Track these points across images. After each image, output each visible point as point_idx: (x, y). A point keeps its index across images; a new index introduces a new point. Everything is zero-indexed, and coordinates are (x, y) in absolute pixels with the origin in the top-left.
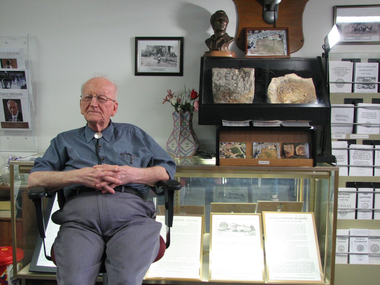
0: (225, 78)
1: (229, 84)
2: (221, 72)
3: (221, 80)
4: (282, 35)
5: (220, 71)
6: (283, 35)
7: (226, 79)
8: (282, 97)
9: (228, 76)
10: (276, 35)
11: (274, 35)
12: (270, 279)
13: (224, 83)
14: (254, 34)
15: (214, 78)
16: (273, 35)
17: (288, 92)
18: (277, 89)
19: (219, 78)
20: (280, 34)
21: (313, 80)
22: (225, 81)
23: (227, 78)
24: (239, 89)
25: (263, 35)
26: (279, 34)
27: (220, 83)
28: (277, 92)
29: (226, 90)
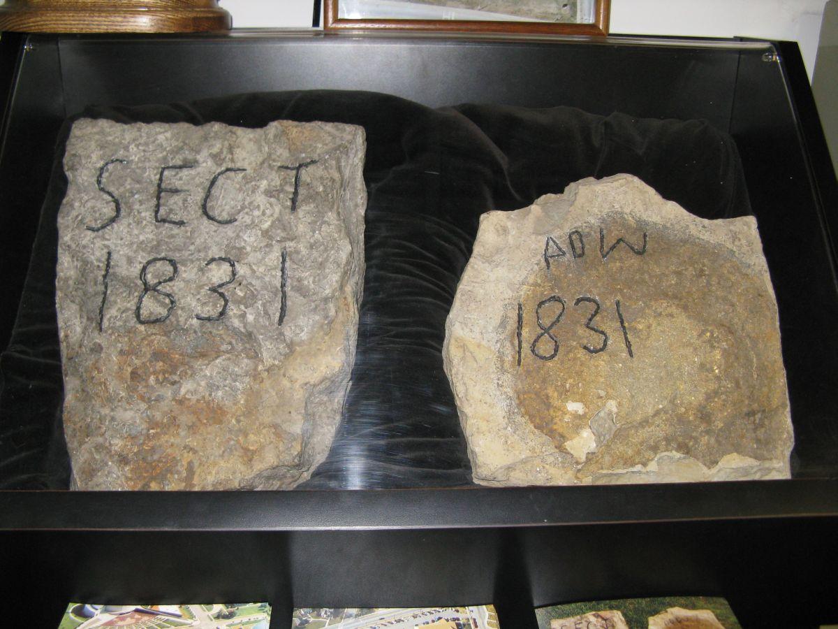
0: (154, 201)
1: (173, 263)
2: (135, 154)
3: (120, 227)
4: (468, 619)
5: (126, 148)
6: (471, 622)
7: (162, 211)
8: (550, 391)
9: (178, 184)
10: (443, 621)
11: (433, 621)
12: (235, 25)
13: (141, 246)
14: (338, 619)
15: (77, 204)
16: (428, 623)
17: (597, 341)
18: (513, 315)
19: (109, 211)
20: (458, 619)
21: (762, 228)
22: (148, 234)
23: (175, 201)
24: (243, 316)
25: (383, 622)
26: (454, 620)
27: (114, 256)
28: (516, 342)
29: (142, 328)
